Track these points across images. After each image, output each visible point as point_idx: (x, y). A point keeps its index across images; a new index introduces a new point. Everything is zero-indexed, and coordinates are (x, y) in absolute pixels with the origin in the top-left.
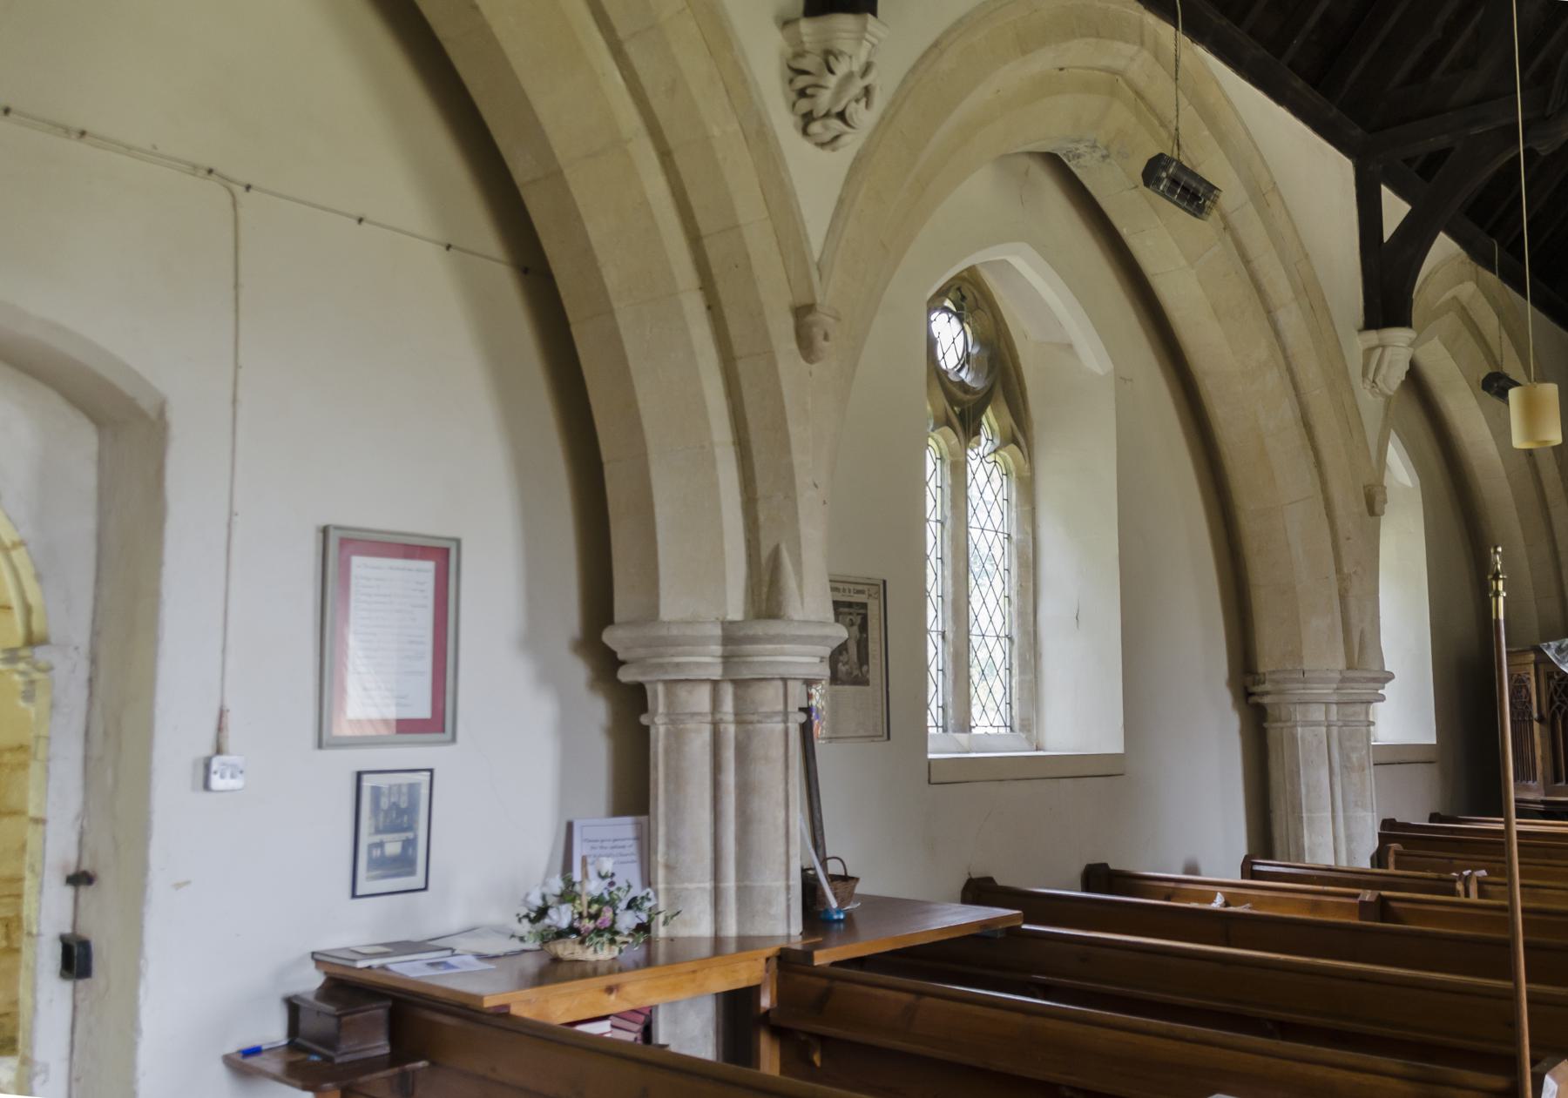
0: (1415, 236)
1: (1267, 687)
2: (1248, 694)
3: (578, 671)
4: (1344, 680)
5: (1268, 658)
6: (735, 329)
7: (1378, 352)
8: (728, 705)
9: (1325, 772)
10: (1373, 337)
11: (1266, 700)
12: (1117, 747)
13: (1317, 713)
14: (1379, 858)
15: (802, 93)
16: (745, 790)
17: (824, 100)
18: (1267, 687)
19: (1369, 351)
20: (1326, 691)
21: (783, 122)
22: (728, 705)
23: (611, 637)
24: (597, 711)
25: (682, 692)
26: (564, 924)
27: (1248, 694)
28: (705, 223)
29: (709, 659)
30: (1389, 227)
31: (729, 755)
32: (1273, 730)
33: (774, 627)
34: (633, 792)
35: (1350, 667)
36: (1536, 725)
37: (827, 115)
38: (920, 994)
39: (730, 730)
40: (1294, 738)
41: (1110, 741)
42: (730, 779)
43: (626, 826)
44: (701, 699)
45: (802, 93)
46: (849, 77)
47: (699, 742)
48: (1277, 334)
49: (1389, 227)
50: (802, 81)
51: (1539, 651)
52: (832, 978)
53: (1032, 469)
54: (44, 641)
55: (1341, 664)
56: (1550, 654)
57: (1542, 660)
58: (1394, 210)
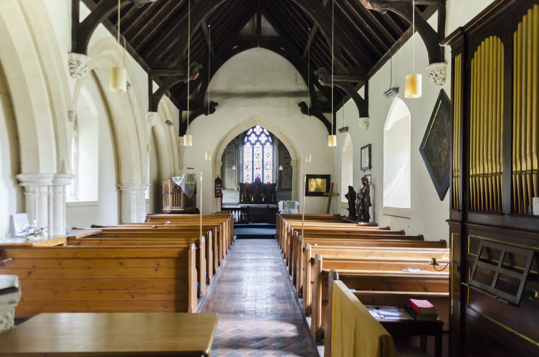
0: (160, 93)
1: (124, 186)
2: (119, 188)
3: (11, 183)
4: (141, 185)
5: (125, 179)
6: (57, 114)
7: (151, 117)
8: (51, 190)
9: (136, 205)
10: (150, 113)
11: (123, 189)
12: (96, 199)
13: (135, 192)
14: (146, 221)
15: (71, 68)
16: (55, 207)
17: (77, 71)
18: (124, 186)
19: (149, 116)
20: (137, 187)
21: (68, 73)
22: (51, 190)
23: (21, 177)
24: (14, 191)
25: (42, 188)
26: (32, 233)
27: (119, 188)
28: (53, 93)
29: (49, 182)
30: (154, 91)
31: (51, 201)
32: (124, 196)
33: (62, 175)
34: (23, 208)
35: (142, 183)
36: (170, 195)
37: (78, 74)
38: (101, 240)
39: (51, 195)
40: (130, 198)
41: (94, 198)
42: (51, 205)
43: (24, 216)
44: (45, 189)
45: (71, 68)
46: (83, 68)
47: (45, 198)
48: (133, 111)
49: (154, 91)
50: (72, 66)
51: (171, 179)
52: (80, 240)
53: (78, 136)
54: (20, 182)
55: (140, 182)
56: (174, 180)
57: (172, 181)
58: (156, 87)
